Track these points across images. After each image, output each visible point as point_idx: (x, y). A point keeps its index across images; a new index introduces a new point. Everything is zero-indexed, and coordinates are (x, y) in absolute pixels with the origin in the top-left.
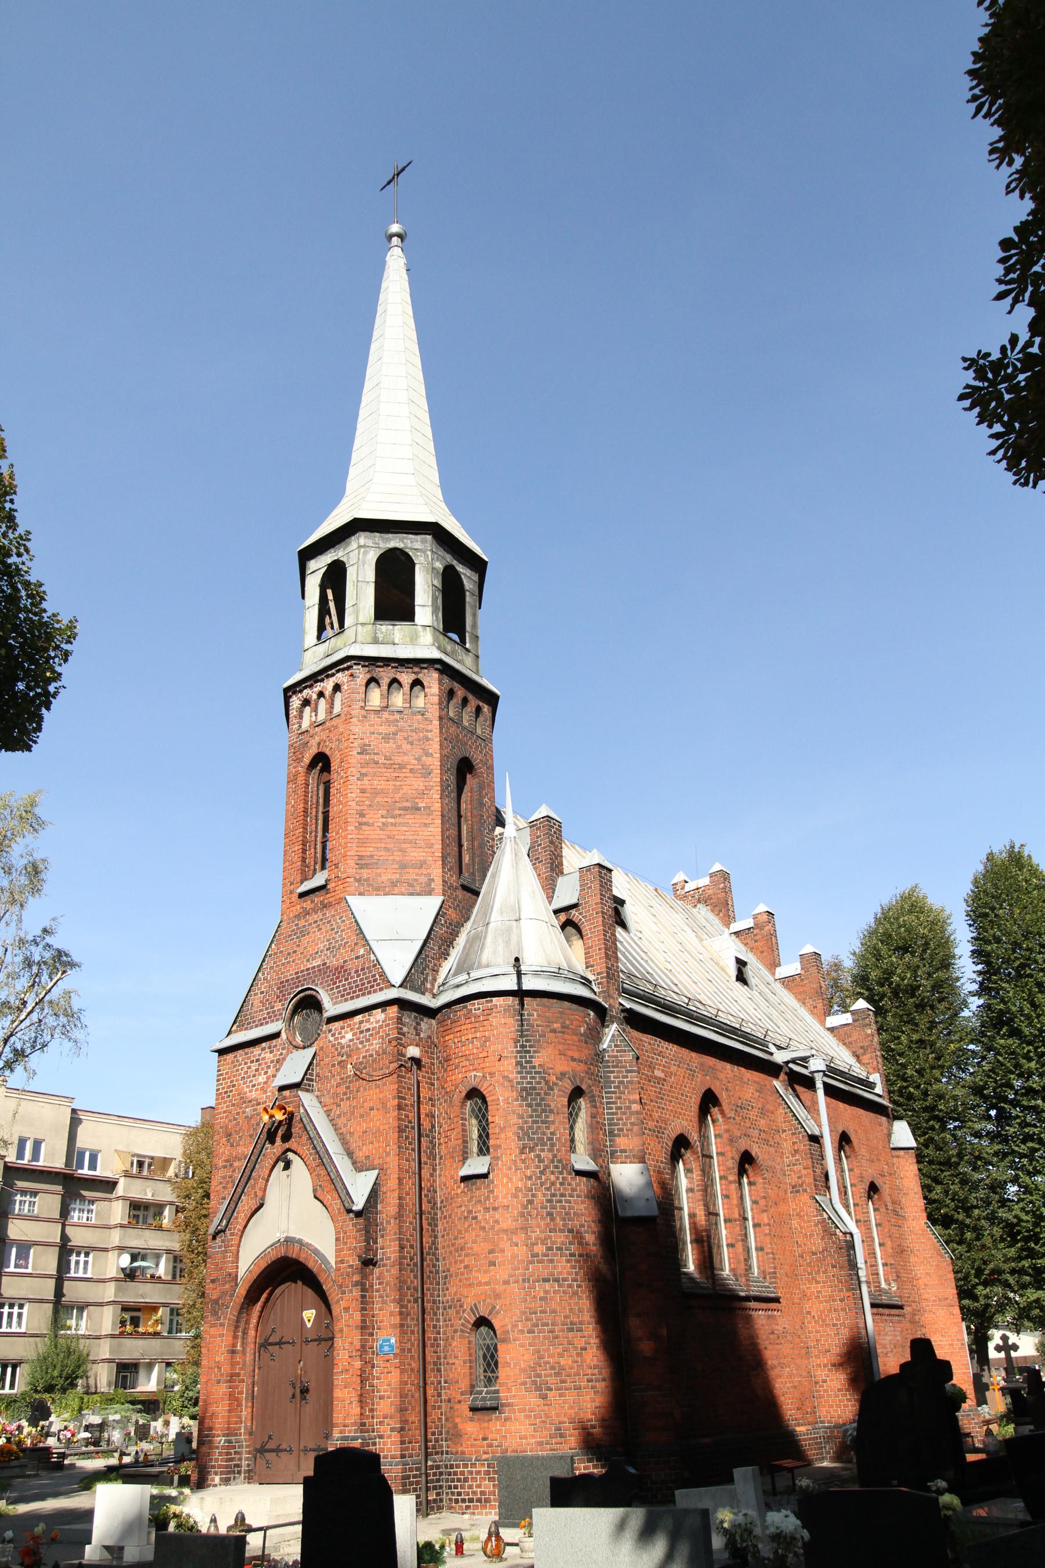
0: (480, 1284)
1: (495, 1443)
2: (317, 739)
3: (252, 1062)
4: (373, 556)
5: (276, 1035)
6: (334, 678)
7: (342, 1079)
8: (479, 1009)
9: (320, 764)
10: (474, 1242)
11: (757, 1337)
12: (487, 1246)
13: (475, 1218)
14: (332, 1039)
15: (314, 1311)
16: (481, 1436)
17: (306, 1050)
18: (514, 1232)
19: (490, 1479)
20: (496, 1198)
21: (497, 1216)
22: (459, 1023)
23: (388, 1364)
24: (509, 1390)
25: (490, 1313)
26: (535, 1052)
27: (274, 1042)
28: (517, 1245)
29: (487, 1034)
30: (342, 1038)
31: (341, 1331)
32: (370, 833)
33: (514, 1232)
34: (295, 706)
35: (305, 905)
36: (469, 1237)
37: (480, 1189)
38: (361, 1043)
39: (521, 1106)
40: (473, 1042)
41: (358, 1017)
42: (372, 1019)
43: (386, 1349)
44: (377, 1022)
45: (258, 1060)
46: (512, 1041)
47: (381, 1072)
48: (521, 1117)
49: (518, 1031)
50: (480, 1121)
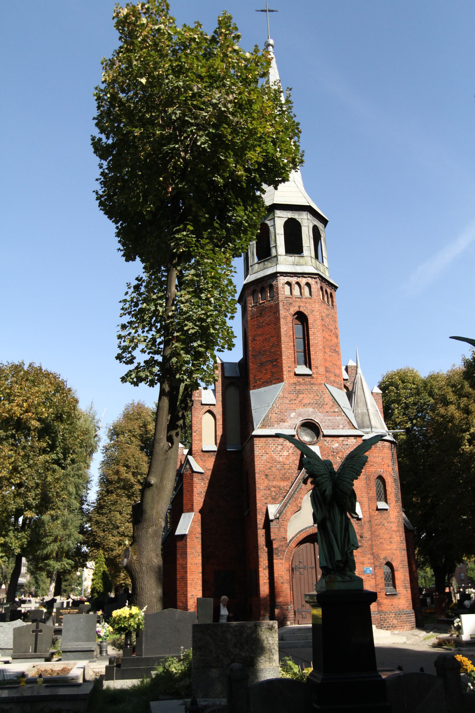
0: (387, 549)
1: (396, 607)
2: (298, 304)
3: (279, 445)
4: (284, 220)
6: (306, 279)
10: (383, 534)
11: (161, 598)
12: (389, 536)
13: (383, 525)
14: (326, 444)
18: (396, 531)
23: (369, 578)
24: (399, 588)
25: (391, 560)
30: (333, 445)
34: (282, 282)
35: (299, 380)
36: (382, 531)
37: (385, 514)
38: (344, 449)
41: (341, 438)
43: (368, 572)
44: (352, 442)
45: (281, 445)
48: (395, 489)
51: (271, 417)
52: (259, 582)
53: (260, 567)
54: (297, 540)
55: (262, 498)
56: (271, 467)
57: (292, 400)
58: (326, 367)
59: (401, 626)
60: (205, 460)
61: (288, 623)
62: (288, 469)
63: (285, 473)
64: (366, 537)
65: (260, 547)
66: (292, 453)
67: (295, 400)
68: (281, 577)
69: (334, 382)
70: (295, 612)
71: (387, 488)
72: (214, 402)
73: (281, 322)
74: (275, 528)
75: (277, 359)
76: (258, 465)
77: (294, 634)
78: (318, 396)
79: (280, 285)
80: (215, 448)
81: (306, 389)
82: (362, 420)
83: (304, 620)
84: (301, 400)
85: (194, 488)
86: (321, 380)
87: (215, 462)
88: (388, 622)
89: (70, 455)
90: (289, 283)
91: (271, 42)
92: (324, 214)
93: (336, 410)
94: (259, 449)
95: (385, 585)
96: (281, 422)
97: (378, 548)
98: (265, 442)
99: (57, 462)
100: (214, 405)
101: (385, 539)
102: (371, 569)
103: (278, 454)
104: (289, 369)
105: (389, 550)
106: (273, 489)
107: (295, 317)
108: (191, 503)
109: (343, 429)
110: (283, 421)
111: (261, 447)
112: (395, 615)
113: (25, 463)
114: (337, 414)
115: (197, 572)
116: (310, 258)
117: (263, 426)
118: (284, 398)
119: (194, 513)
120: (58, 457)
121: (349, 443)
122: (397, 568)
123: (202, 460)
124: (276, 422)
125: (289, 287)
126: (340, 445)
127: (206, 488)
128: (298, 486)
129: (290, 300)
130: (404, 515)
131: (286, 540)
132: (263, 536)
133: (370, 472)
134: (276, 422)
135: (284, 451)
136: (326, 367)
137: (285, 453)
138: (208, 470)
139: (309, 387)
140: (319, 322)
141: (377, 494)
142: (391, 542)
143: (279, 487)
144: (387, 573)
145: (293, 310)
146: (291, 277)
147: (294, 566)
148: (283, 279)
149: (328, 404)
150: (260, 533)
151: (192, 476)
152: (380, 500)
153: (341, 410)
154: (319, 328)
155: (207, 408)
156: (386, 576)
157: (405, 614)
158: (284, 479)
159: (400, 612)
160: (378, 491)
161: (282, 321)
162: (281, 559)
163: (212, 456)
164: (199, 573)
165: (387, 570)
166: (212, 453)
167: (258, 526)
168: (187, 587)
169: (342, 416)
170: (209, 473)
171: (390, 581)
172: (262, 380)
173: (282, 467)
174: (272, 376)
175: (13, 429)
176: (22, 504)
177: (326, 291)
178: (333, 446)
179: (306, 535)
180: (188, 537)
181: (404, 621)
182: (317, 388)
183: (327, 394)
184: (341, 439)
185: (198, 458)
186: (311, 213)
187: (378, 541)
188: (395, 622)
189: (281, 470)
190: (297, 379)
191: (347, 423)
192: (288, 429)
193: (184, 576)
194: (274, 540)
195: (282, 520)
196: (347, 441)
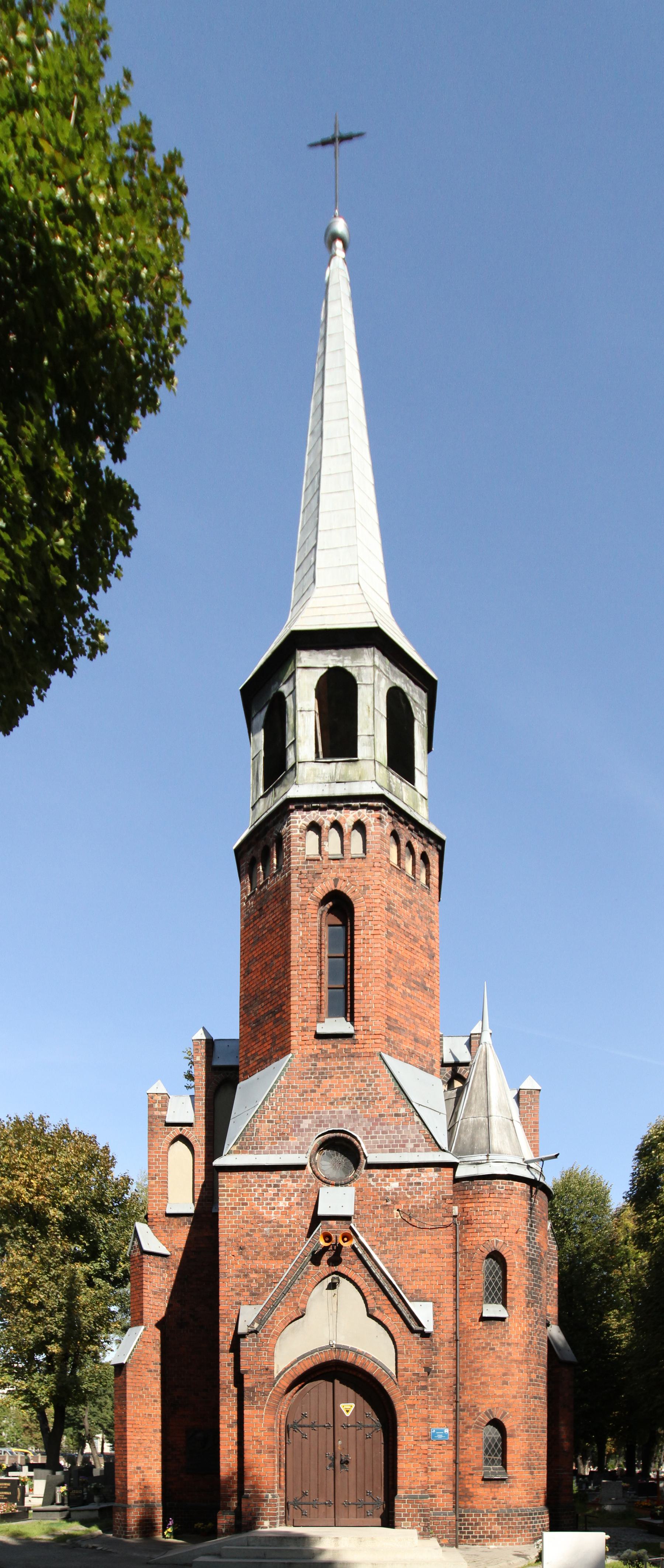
0: (495, 1396)
1: (503, 1501)
2: (333, 874)
3: (270, 1186)
5: (302, 1167)
6: (356, 812)
7: (387, 1221)
8: (502, 1188)
9: (331, 903)
10: (490, 1366)
12: (502, 1370)
13: (493, 1349)
14: (372, 1183)
15: (353, 1405)
16: (491, 1497)
17: (339, 1188)
18: (521, 1362)
19: (499, 1524)
20: (510, 1337)
21: (510, 1350)
22: (482, 1196)
23: (441, 1447)
24: (513, 1468)
26: (537, 1232)
27: (298, 1173)
28: (522, 1372)
29: (508, 1209)
30: (386, 1185)
31: (406, 1421)
32: (395, 996)
33: (521, 1362)
34: (299, 825)
35: (323, 1047)
36: (487, 1362)
38: (411, 1193)
39: (528, 1271)
40: (496, 1214)
41: (406, 1170)
42: (423, 1175)
43: (440, 1437)
45: (275, 1186)
46: (525, 1220)
47: (433, 1223)
48: (528, 1280)
49: (528, 1213)
50: (487, 1277)
51: (258, 1130)
52: (219, 1449)
53: (221, 1421)
54: (292, 1373)
55: (230, 1294)
56: (251, 1231)
57: (306, 1092)
58: (389, 1018)
59: (509, 1536)
60: (172, 1232)
61: (266, 1523)
62: (287, 1235)
63: (281, 1244)
64: (443, 1371)
65: (222, 1386)
66: (297, 1204)
67: (314, 1091)
68: (257, 1441)
69: (412, 1054)
70: (287, 1504)
71: (508, 1277)
72: (190, 1119)
73: (292, 920)
74: (249, 1349)
75: (282, 1005)
76: (225, 1227)
77: (248, 1545)
78: (365, 1081)
79: (295, 832)
80: (191, 1209)
81: (340, 1068)
82: (473, 1137)
83: (305, 1518)
84: (327, 1091)
85: (144, 1283)
86: (371, 1046)
87: (190, 1235)
88: (481, 1528)
89: (121, 1264)
90: (315, 827)
91: (340, 226)
92: (428, 665)
93: (402, 1111)
94: (228, 1195)
95: (486, 1461)
96: (279, 1139)
97: (476, 1392)
98: (240, 1182)
99: (100, 1274)
100: (190, 1125)
101: (493, 1376)
102: (447, 1431)
103: (267, 1204)
104: (305, 1024)
105: (500, 1396)
106: (253, 1275)
107: (328, 906)
108: (140, 1310)
109: (413, 1151)
110: (284, 1136)
111: (232, 1191)
112: (498, 1515)
113: (46, 1273)
114: (402, 1119)
115: (151, 1430)
116: (372, 763)
117: (241, 1148)
118: (288, 1087)
119: (143, 1327)
120: (101, 1266)
121: (422, 1181)
122: (513, 1430)
123: (166, 1231)
124: (269, 1139)
125: (317, 837)
126: (403, 1184)
127: (172, 1283)
128: (302, 1269)
129: (317, 868)
130: (555, 1331)
131: (272, 1372)
132: (229, 1364)
133: (474, 1243)
134: (269, 1139)
135: (281, 1200)
136: (389, 1018)
137: (284, 1203)
138: (176, 1250)
139: (345, 1062)
140: (379, 914)
141: (487, 1289)
142: (505, 1383)
143: (266, 1271)
144: (493, 1440)
145: (322, 889)
146: (323, 809)
147: (290, 1423)
148: (303, 817)
149: (384, 1098)
150: (224, 1360)
151: (141, 1260)
152: (493, 1301)
153: (412, 1110)
154: (379, 927)
155: (177, 1131)
156: (490, 1446)
157: (519, 1515)
158: (278, 1254)
159: (510, 1511)
160: (490, 1284)
161: (295, 916)
162: (258, 1408)
163: (185, 1224)
164: (155, 1431)
165: (493, 1435)
166: (185, 1219)
167: (221, 1346)
168: (126, 1455)
169: (413, 1122)
170: (179, 1255)
171: (496, 1455)
172: (258, 1058)
173: (275, 1231)
174: (273, 1044)
175: (24, 1223)
176: (41, 1334)
177: (409, 845)
178: (387, 1188)
179: (312, 1365)
180: (128, 1369)
181: (516, 1528)
182: (362, 1064)
183: (384, 1076)
184: (406, 1171)
185: (159, 1228)
186: (384, 654)
187: (477, 1379)
188: (497, 1528)
189: (272, 1237)
190: (319, 1047)
191: (423, 1138)
192: (294, 1153)
193: (123, 1436)
194: (246, 1372)
195: (265, 1336)
196: (419, 1176)
